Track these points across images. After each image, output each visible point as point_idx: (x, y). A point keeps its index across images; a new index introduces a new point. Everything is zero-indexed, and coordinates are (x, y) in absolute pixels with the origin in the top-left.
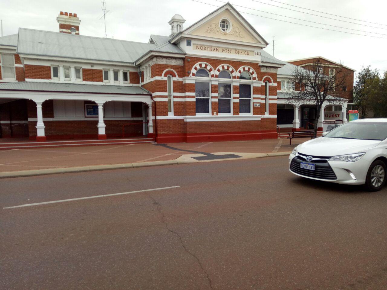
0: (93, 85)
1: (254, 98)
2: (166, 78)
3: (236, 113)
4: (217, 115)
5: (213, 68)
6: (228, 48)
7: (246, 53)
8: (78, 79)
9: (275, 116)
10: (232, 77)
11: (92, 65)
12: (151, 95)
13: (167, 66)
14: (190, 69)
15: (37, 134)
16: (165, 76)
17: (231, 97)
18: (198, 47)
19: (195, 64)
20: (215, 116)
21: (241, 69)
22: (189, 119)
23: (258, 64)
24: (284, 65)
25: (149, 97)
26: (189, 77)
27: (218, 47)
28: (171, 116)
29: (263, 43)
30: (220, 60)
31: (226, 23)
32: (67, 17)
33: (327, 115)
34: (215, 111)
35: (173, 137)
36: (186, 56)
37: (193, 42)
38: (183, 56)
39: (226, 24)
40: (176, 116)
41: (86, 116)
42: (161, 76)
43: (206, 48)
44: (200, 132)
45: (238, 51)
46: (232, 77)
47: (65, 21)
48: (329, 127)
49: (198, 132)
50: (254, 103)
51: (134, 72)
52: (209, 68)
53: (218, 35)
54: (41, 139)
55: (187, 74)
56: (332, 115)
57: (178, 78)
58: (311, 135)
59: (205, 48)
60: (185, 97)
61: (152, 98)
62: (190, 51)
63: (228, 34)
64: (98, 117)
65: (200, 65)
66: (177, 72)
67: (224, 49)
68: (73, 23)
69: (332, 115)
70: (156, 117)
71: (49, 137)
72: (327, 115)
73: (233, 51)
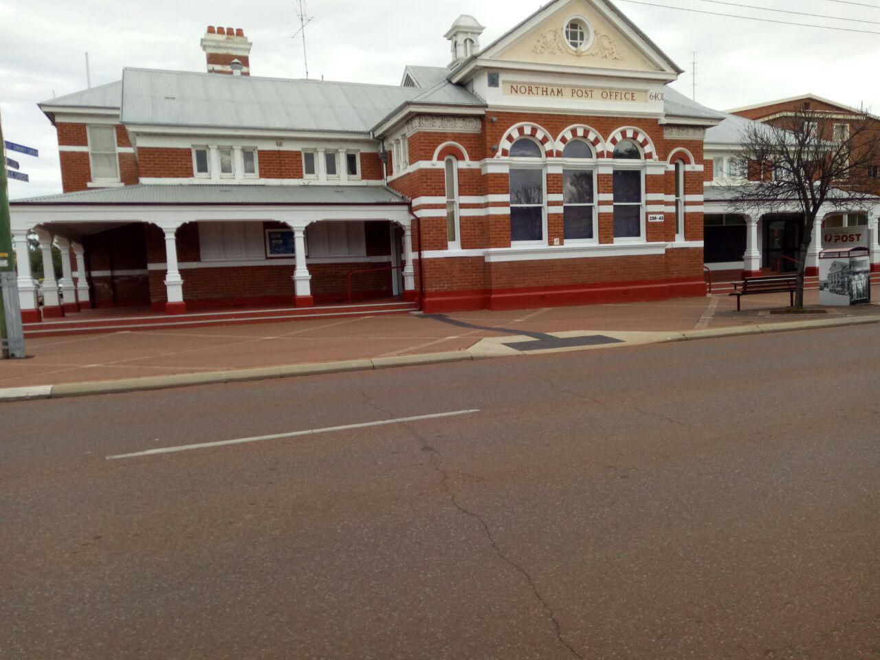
0: (282, 186)
1: (648, 203)
2: (441, 165)
3: (605, 238)
4: (562, 243)
5: (550, 136)
6: (584, 87)
7: (628, 96)
8: (250, 175)
9: (700, 244)
10: (594, 155)
11: (279, 141)
12: (409, 204)
13: (443, 137)
14: (497, 140)
15: (166, 298)
16: (440, 158)
17: (640, 201)
18: (515, 89)
19: (508, 127)
20: (556, 246)
21: (616, 134)
22: (496, 255)
23: (657, 120)
24: (721, 119)
25: (406, 208)
26: (495, 158)
27: (561, 85)
28: (455, 250)
29: (668, 70)
30: (566, 116)
31: (580, 29)
32: (222, 37)
33: (828, 238)
34: (555, 237)
35: (467, 297)
36: (487, 110)
37: (502, 77)
38: (481, 112)
39: (579, 31)
40: (465, 251)
41: (269, 255)
42: (430, 158)
43: (534, 90)
44: (521, 286)
45: (584, 91)
46: (594, 155)
47: (220, 47)
48: (835, 265)
49: (516, 286)
50: (647, 214)
51: (370, 154)
52: (540, 135)
53: (563, 58)
54: (176, 308)
55: (490, 152)
56: (841, 235)
57: (470, 162)
58: (789, 285)
59: (530, 90)
60: (487, 205)
61: (411, 211)
62: (496, 98)
63: (585, 54)
64: (294, 257)
65: (521, 130)
66: (467, 148)
67: (577, 90)
68: (236, 49)
69: (841, 235)
70: (420, 255)
71: (192, 303)
72: (828, 238)
73: (597, 93)
